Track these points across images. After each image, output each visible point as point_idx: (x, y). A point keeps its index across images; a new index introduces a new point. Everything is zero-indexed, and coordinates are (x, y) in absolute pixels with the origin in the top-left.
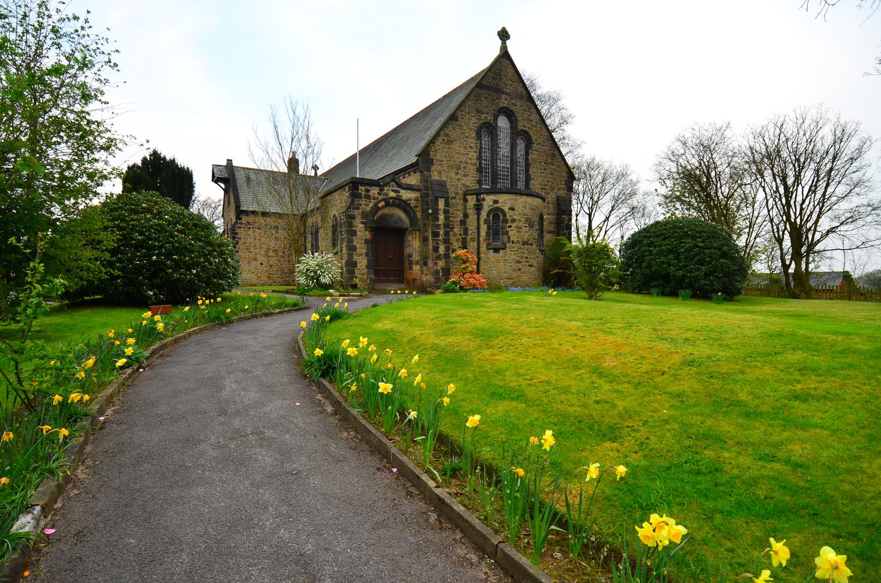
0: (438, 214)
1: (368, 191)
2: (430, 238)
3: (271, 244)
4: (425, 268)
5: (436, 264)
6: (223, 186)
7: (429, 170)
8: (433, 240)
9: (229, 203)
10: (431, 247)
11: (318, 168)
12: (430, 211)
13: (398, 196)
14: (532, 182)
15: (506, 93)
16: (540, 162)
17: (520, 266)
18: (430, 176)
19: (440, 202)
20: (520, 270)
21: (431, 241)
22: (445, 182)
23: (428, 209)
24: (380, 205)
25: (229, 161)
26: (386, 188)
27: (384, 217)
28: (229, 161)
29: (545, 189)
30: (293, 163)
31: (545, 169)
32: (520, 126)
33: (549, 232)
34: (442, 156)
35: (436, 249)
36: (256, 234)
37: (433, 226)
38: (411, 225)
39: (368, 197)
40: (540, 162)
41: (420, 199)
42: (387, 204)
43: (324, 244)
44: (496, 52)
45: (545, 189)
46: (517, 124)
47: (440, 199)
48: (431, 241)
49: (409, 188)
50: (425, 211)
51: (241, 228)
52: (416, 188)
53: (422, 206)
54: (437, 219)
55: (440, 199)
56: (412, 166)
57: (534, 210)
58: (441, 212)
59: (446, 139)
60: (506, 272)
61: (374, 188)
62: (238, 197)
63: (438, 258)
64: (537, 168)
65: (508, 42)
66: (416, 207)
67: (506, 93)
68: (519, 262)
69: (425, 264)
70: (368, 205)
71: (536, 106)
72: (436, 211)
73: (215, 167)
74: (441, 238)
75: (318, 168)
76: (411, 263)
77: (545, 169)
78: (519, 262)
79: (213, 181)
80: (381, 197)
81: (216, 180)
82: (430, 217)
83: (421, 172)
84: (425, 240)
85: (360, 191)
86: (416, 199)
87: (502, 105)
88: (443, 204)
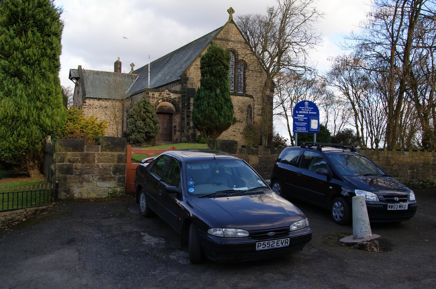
0: (190, 106)
1: (153, 95)
2: (186, 118)
3: (102, 118)
4: (182, 134)
5: (188, 132)
6: (75, 81)
7: (186, 83)
8: (187, 119)
9: (78, 92)
10: (186, 123)
11: (134, 65)
12: (186, 104)
13: (169, 96)
14: (247, 87)
15: (232, 41)
16: (253, 76)
17: (235, 133)
18: (187, 86)
19: (191, 100)
20: (234, 135)
21: (186, 120)
22: (194, 89)
23: (185, 103)
24: (159, 101)
25: (80, 67)
26: (163, 93)
27: (162, 107)
28: (80, 67)
29: (256, 91)
30: (118, 65)
31: (256, 80)
32: (240, 58)
33: (258, 115)
34: (193, 76)
35: (188, 124)
36: (94, 112)
37: (187, 112)
38: (176, 111)
39: (153, 98)
40: (253, 76)
41: (181, 98)
42: (163, 101)
43: (166, 103)
44: (227, 20)
45: (256, 91)
46: (238, 57)
47: (191, 98)
48: (186, 120)
49: (175, 92)
50: (183, 104)
51: (85, 108)
52: (179, 92)
53: (182, 101)
54: (189, 108)
55: (191, 98)
56: (178, 81)
57: (244, 103)
58: (192, 105)
59: (196, 67)
60: (226, 137)
61: (157, 93)
62: (85, 90)
63: (190, 128)
64: (251, 79)
65: (233, 15)
66: (179, 102)
67: (232, 41)
68: (234, 131)
69: (183, 131)
70: (153, 101)
71: (174, 93)
72: (189, 104)
73: (71, 71)
74: (191, 118)
75: (134, 65)
76: (175, 131)
77: (256, 80)
78: (234, 131)
79: (69, 78)
80: (160, 97)
81: (71, 78)
82: (186, 107)
83: (182, 84)
84: (183, 119)
85: (149, 95)
86: (179, 98)
87: (229, 47)
88: (193, 101)
